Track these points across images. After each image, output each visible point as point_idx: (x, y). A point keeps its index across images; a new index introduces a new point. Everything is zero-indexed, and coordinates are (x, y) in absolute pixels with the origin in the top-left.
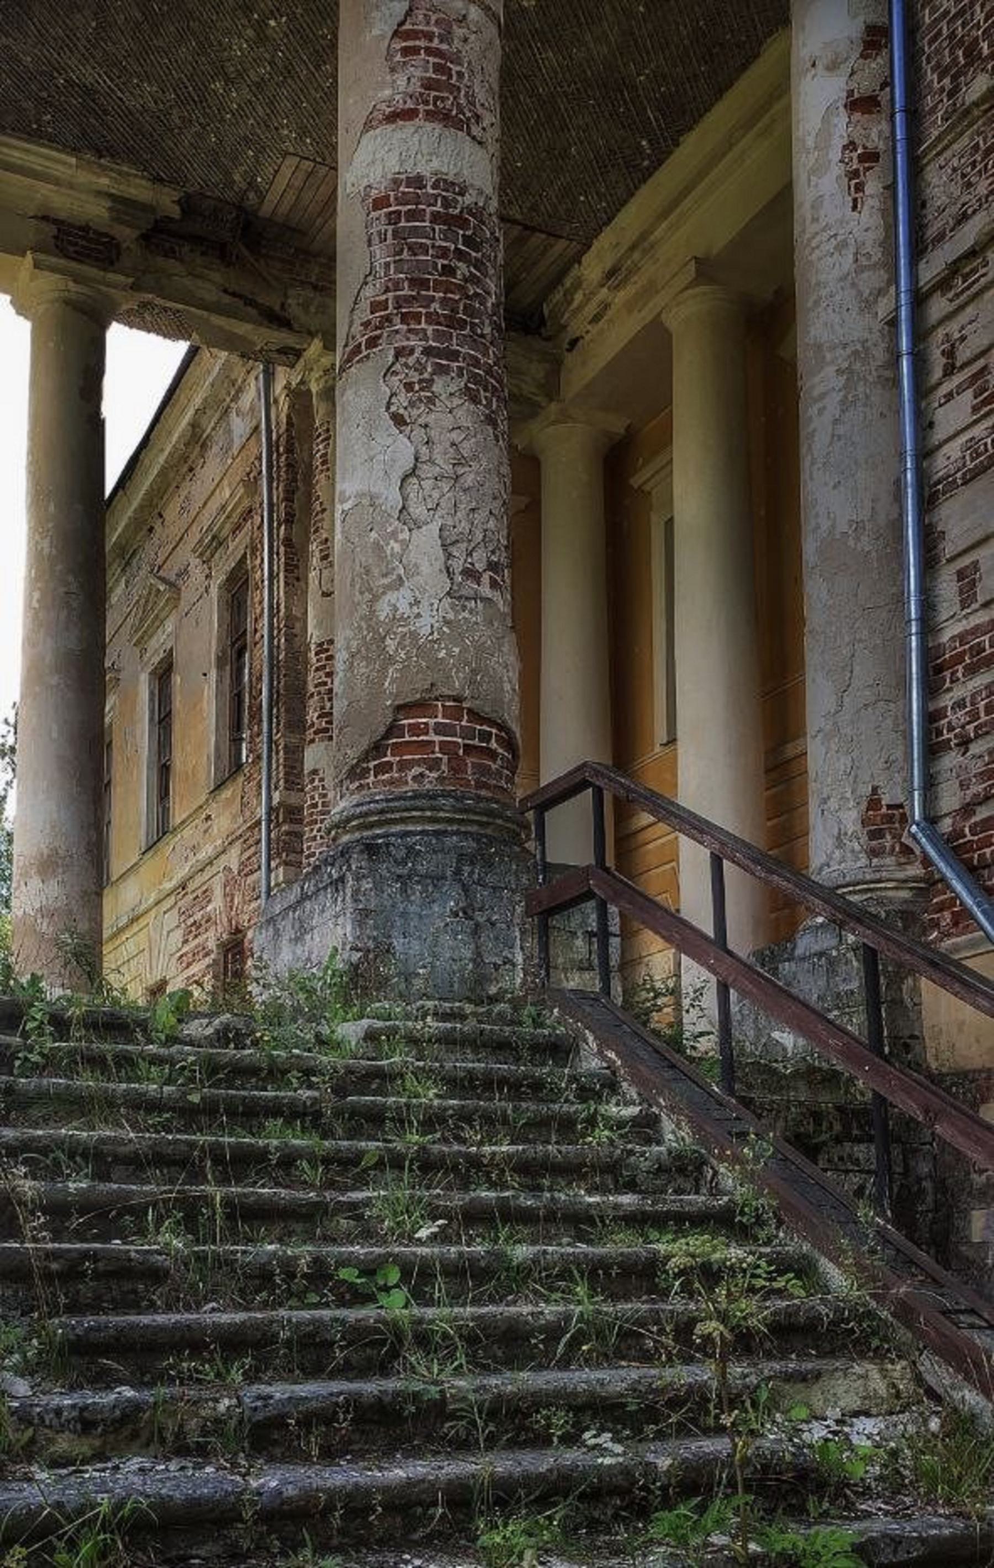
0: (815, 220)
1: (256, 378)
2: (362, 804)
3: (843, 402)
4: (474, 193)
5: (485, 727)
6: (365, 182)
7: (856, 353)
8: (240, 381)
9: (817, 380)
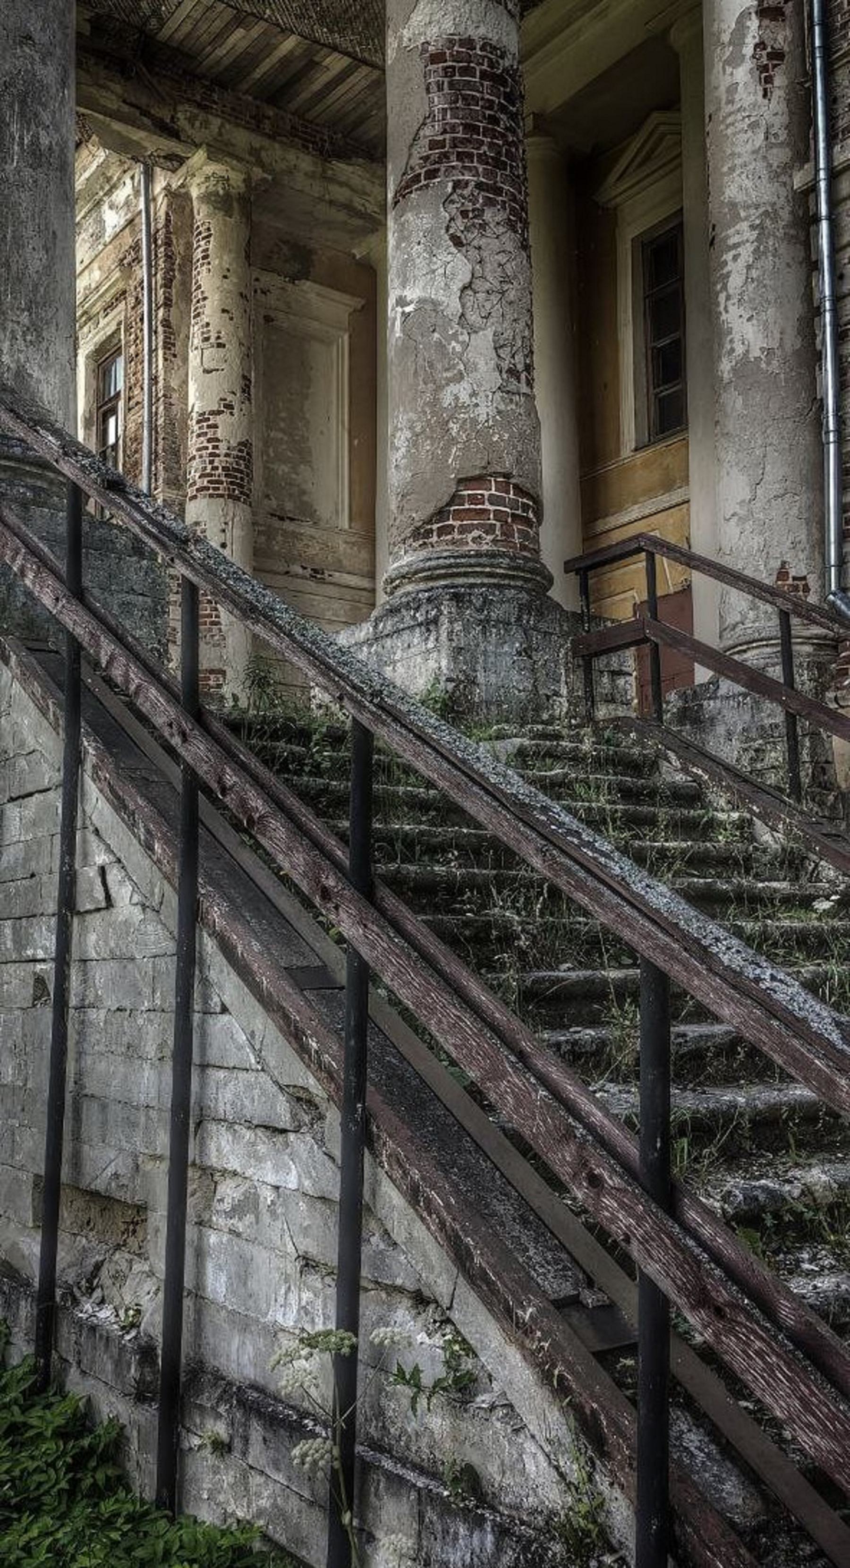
0: (731, 102)
1: (132, 178)
2: (430, 559)
3: (756, 251)
4: (510, 57)
5: (525, 500)
6: (422, 40)
7: (766, 213)
8: (115, 178)
9: (731, 231)
